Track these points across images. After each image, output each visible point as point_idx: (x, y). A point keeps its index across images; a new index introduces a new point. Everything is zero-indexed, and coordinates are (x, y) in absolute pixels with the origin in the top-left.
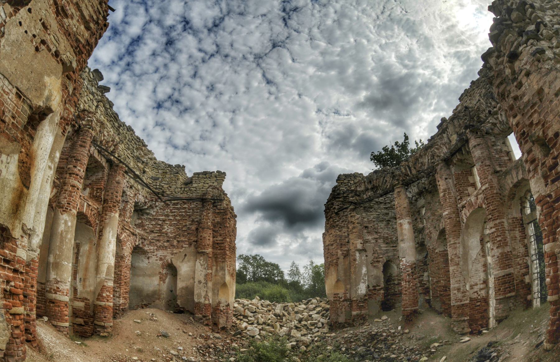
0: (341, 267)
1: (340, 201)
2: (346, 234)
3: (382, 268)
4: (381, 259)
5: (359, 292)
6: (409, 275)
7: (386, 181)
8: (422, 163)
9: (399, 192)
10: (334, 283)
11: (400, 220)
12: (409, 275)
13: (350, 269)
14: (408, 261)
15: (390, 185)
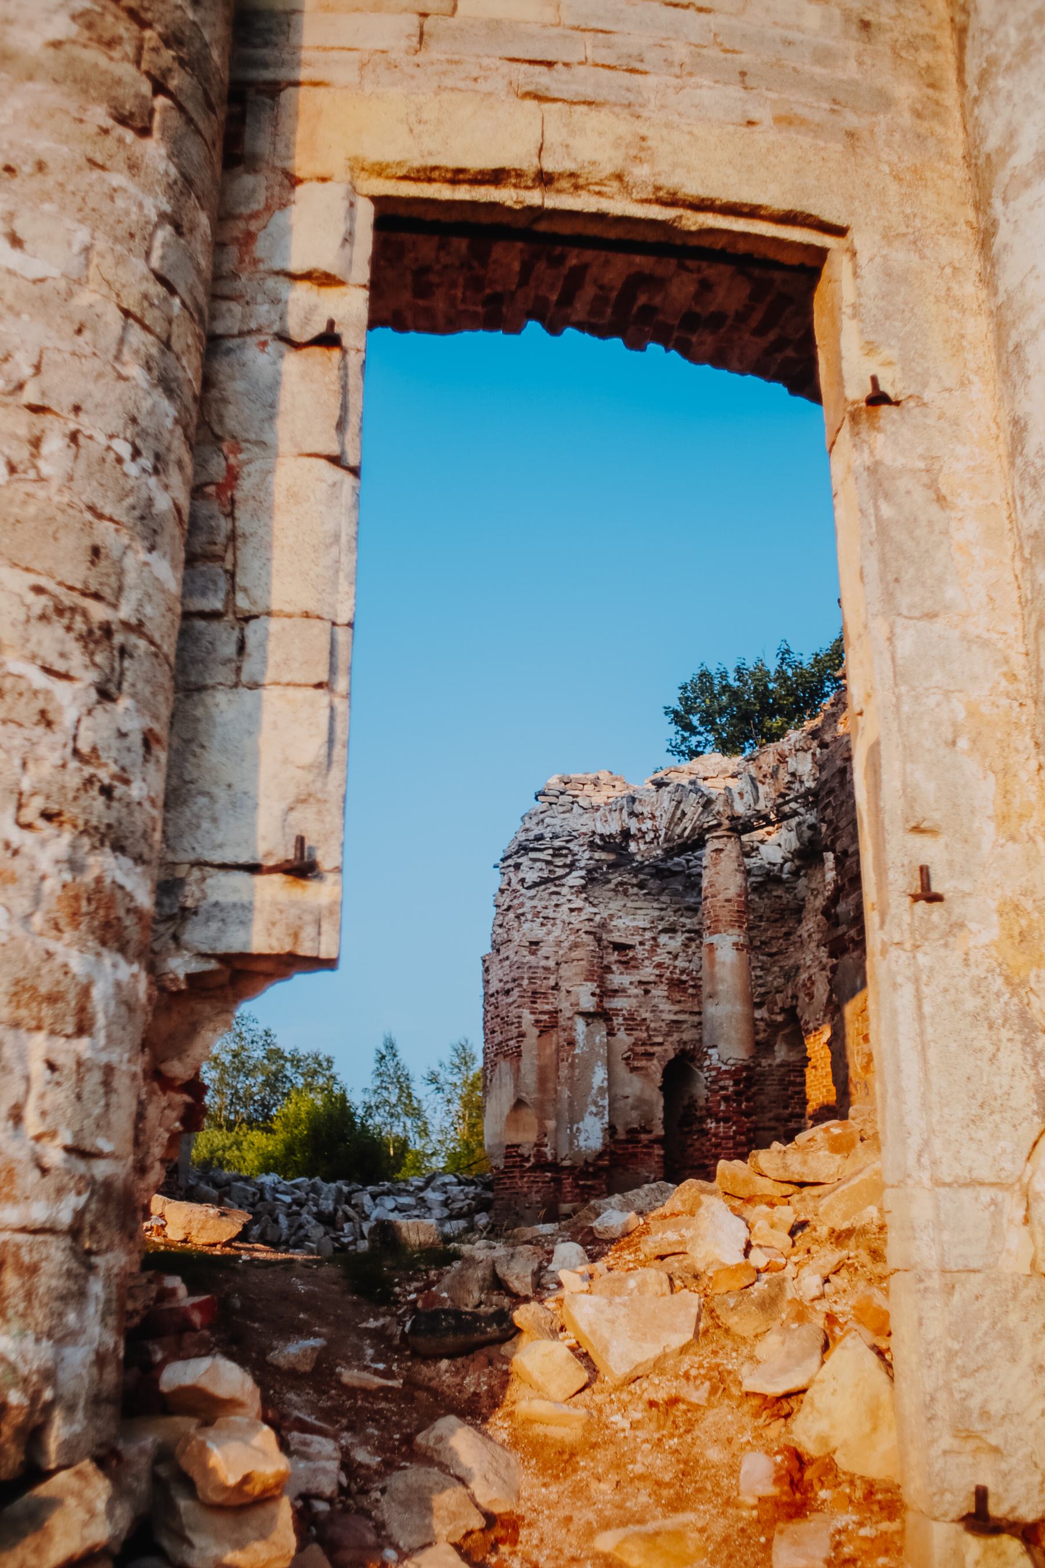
0: (528, 1064)
1: (539, 860)
2: (551, 963)
3: (658, 1077)
4: (656, 1049)
5: (582, 1143)
6: (726, 1099)
7: (684, 814)
8: (793, 774)
9: (718, 851)
10: (506, 1110)
11: (712, 934)
12: (726, 1099)
13: (558, 1070)
14: (724, 1058)
15: (693, 829)
